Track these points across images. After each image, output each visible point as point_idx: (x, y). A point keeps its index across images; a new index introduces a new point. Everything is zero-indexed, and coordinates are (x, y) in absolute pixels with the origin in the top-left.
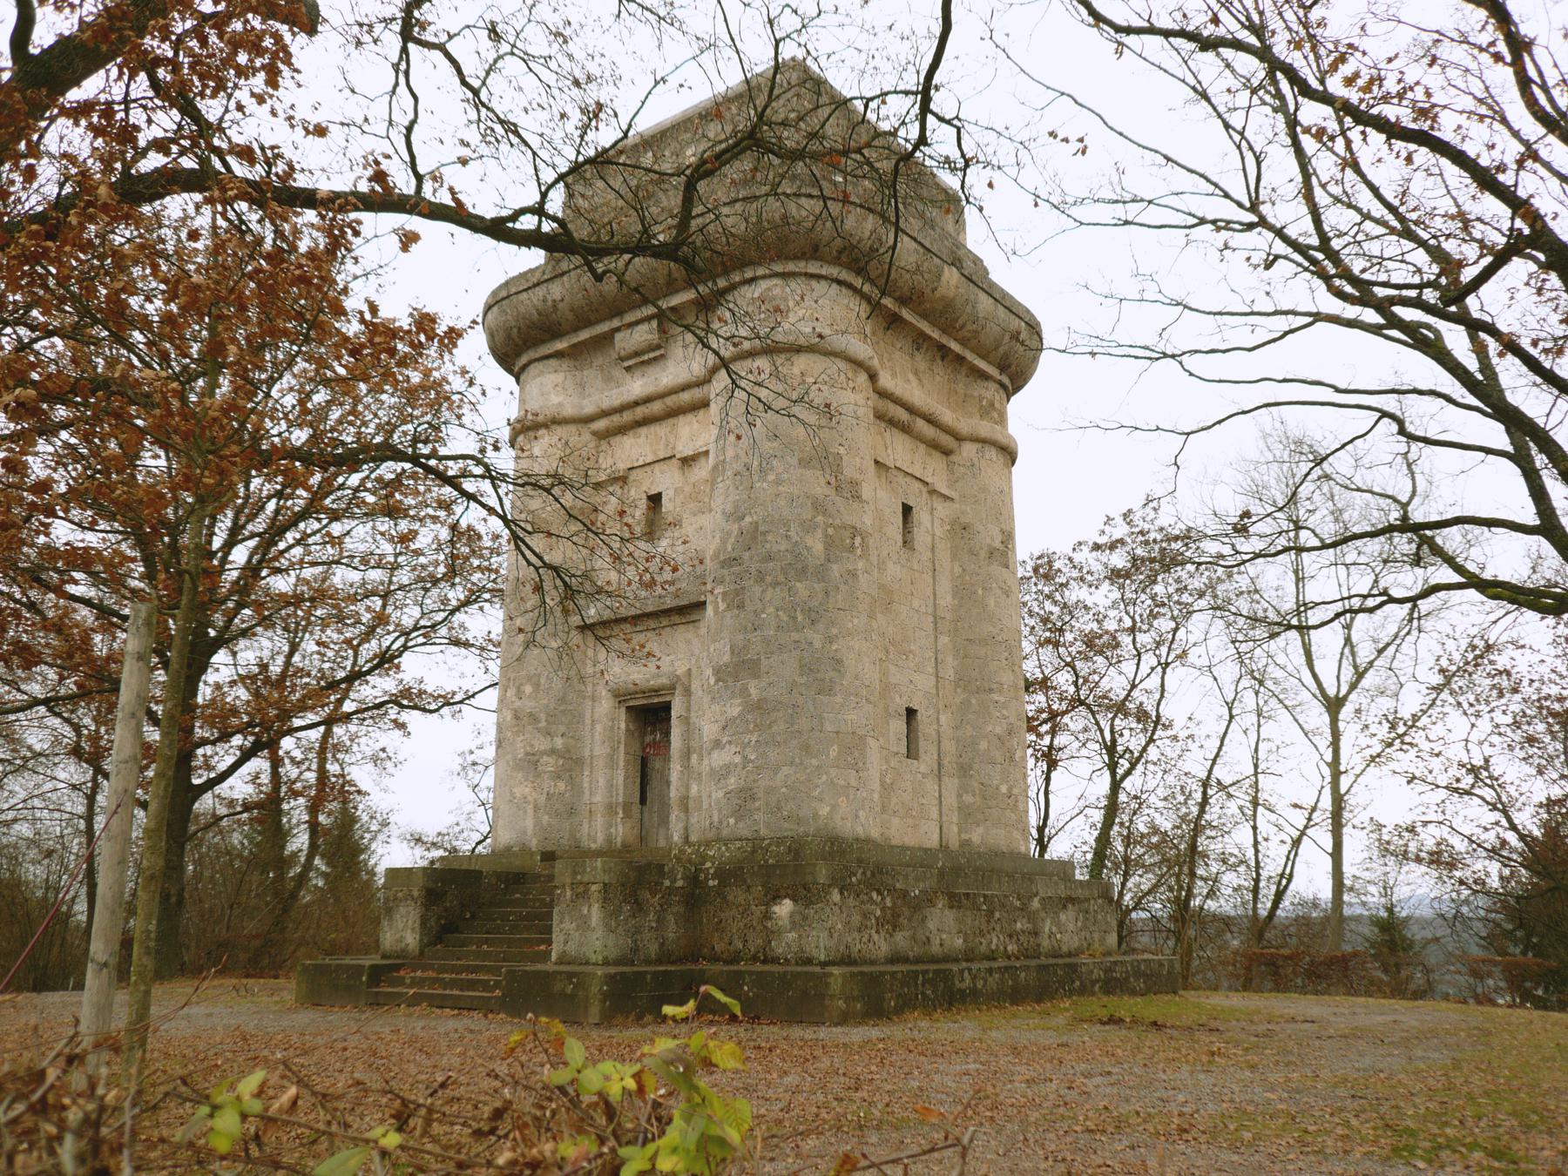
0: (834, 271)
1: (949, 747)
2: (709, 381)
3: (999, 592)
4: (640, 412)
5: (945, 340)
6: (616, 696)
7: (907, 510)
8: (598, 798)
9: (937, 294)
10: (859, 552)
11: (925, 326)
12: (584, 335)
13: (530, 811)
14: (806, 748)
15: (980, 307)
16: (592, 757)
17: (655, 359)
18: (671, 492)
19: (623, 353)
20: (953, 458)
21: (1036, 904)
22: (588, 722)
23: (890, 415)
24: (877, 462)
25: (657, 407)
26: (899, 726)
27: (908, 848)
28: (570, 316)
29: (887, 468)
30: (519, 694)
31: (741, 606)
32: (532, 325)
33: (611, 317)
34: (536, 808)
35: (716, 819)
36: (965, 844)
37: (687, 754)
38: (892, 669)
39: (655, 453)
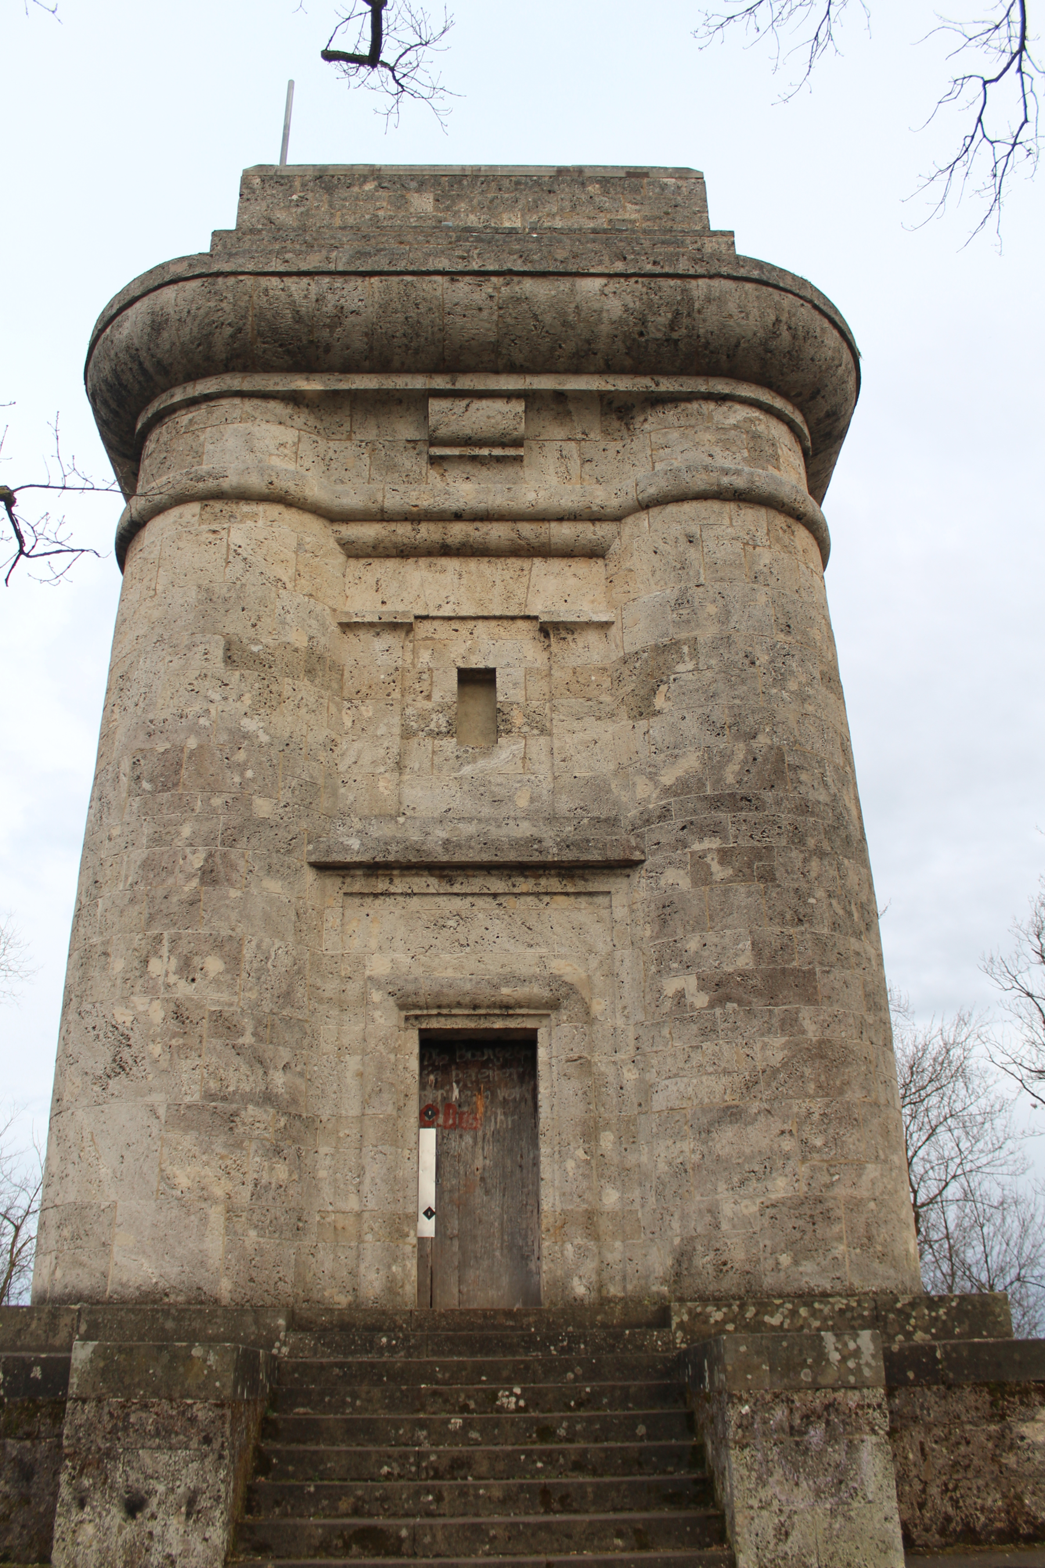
6: (402, 1007)
13: (216, 1215)
17: (499, 459)
18: (518, 674)
19: (443, 432)
22: (329, 1048)
25: (497, 533)
28: (359, 343)
34: (231, 1213)
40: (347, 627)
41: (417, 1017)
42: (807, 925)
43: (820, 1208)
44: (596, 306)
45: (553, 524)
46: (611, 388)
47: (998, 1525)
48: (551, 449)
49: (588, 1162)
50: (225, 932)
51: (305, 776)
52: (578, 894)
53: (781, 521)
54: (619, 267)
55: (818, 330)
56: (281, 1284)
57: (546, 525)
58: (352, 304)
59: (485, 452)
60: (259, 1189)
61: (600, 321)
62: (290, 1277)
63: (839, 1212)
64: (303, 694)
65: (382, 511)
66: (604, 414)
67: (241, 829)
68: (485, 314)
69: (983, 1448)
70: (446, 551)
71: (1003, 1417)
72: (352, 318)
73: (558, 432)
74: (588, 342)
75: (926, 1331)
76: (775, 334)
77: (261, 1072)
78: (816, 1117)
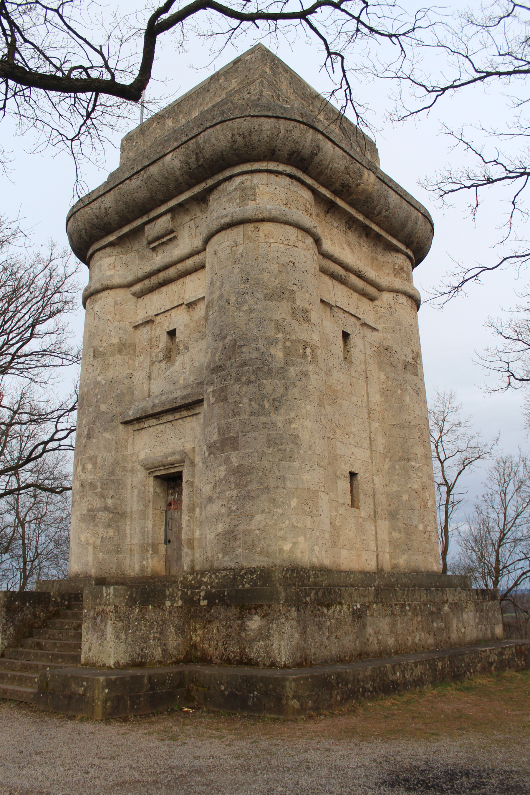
0: (289, 169)
1: (382, 499)
2: (204, 250)
3: (412, 392)
4: (162, 276)
5: (368, 222)
6: (147, 469)
7: (346, 336)
8: (135, 541)
10: (310, 358)
12: (126, 229)
13: (90, 548)
14: (273, 501)
15: (390, 200)
16: (132, 512)
17: (170, 240)
18: (182, 328)
20: (376, 303)
21: (446, 608)
22: (129, 487)
23: (332, 270)
24: (322, 301)
25: (172, 272)
26: (344, 485)
27: (352, 572)
28: (116, 217)
29: (331, 307)
30: (84, 469)
32: (94, 226)
33: (141, 215)
34: (95, 548)
35: (209, 554)
36: (395, 566)
37: (192, 509)
38: (339, 444)
39: (172, 302)
40: (136, 327)
41: (152, 472)
42: (237, 417)
43: (232, 535)
44: (171, 166)
45: (187, 261)
46: (192, 194)
47: (237, 658)
48: (187, 228)
49: (189, 520)
50: (93, 454)
51: (119, 392)
52: (192, 415)
54: (176, 144)
55: (257, 126)
56: (111, 570)
58: (107, 206)
59: (164, 240)
60: (103, 539)
61: (175, 171)
62: (115, 567)
63: (240, 536)
64: (117, 360)
65: (138, 278)
66: (198, 204)
67: (96, 417)
68: (142, 188)
69: (236, 630)
70: (161, 285)
71: (243, 618)
72: (110, 210)
73: (187, 218)
74: (176, 181)
75: (249, 584)
76: (235, 142)
77: (103, 500)
78: (234, 497)
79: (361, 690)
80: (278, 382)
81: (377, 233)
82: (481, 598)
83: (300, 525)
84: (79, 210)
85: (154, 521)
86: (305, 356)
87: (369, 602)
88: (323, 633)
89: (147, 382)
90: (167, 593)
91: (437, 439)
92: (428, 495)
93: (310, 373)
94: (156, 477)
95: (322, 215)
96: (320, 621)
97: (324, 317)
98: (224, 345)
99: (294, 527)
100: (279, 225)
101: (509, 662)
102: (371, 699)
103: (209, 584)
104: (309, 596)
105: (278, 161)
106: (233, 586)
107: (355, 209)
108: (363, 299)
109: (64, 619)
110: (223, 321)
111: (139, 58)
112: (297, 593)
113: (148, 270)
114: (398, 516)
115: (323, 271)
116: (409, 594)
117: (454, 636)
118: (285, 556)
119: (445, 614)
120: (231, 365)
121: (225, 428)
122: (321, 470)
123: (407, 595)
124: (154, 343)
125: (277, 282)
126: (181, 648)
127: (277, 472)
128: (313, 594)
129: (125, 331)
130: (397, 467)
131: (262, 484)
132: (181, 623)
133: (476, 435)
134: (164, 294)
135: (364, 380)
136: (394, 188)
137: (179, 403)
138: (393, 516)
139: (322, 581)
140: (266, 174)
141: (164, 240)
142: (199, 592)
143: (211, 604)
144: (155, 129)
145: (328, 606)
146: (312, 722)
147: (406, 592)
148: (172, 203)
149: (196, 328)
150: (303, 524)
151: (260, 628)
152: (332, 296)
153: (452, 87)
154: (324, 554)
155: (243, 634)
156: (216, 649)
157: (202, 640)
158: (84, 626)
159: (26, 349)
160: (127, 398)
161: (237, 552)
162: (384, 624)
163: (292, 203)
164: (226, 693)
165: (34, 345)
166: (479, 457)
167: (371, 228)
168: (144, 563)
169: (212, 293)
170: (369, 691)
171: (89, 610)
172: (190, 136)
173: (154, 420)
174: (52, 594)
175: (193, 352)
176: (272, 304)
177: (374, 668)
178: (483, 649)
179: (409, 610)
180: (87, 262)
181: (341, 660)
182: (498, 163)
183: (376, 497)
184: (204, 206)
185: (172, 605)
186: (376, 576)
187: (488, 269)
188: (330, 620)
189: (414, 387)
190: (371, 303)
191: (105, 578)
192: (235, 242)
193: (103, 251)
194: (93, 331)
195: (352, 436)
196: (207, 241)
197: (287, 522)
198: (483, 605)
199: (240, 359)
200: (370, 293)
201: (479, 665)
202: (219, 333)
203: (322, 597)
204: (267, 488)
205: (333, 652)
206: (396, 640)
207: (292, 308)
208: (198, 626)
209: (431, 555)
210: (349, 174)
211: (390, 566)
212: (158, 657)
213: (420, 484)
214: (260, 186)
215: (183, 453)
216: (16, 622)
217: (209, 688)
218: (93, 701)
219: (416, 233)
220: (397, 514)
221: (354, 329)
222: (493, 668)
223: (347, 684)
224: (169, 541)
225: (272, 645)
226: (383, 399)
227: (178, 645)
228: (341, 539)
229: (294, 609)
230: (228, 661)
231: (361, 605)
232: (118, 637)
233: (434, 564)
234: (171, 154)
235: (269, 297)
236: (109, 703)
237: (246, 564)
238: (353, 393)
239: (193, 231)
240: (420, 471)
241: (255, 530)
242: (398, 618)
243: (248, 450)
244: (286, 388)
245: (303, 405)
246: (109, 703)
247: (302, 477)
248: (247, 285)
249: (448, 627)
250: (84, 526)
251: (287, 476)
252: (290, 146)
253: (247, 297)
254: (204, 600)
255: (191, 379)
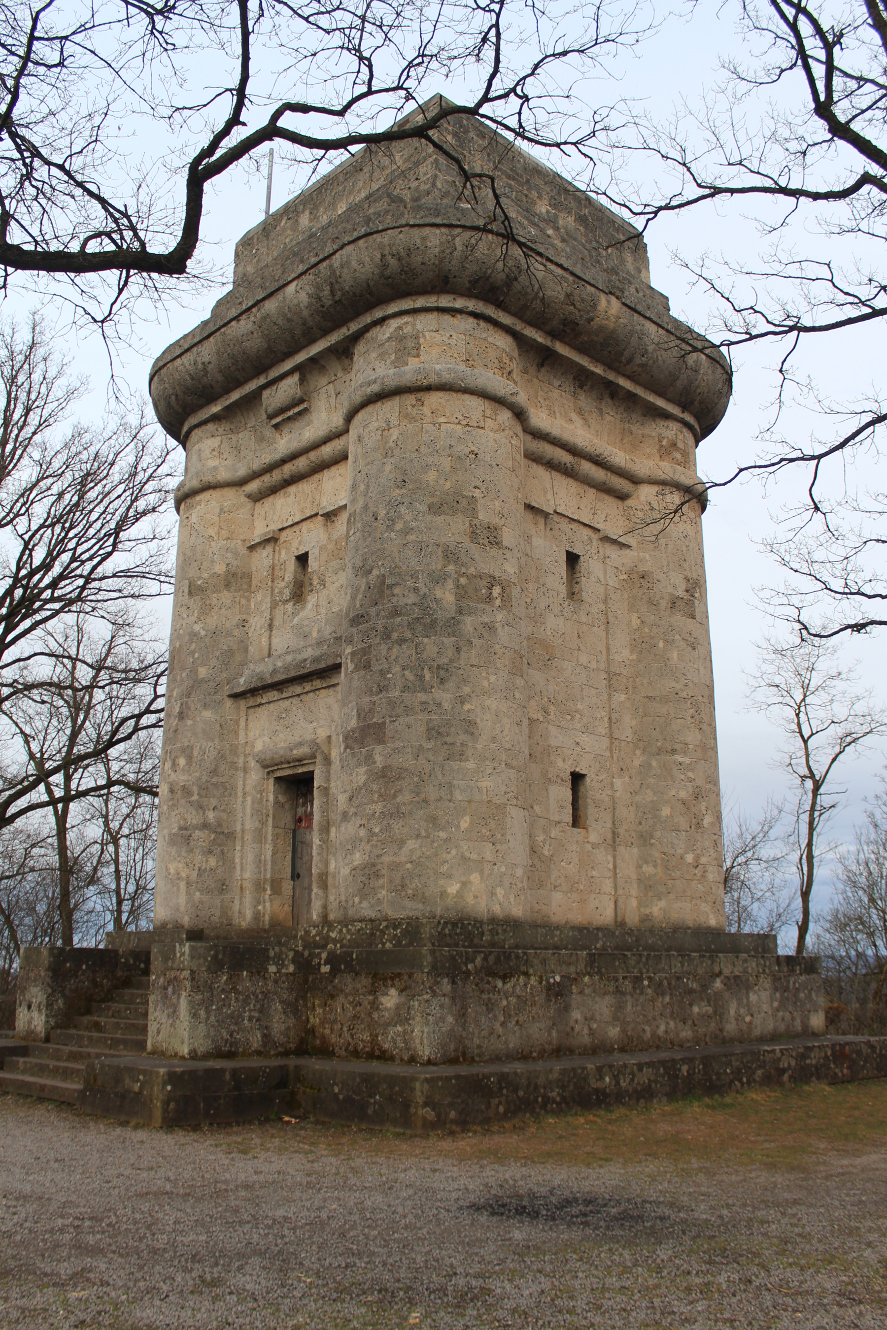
0: (471, 305)
1: (627, 814)
2: (347, 431)
3: (683, 644)
4: (288, 469)
5: (611, 376)
6: (265, 767)
7: (572, 559)
8: (247, 875)
9: (595, 324)
10: (498, 602)
11: (584, 361)
12: (235, 396)
13: (183, 885)
14: (433, 820)
17: (300, 413)
20: (629, 502)
22: (240, 794)
23: (548, 457)
24: (529, 507)
25: (302, 463)
28: (219, 377)
29: (546, 515)
30: (174, 764)
31: (367, 666)
34: (189, 884)
35: (343, 898)
36: (646, 919)
37: (325, 829)
38: (553, 730)
40: (252, 548)
43: (374, 869)
44: (295, 302)
45: (323, 447)
48: (323, 396)
52: (328, 687)
53: (410, 399)
54: (301, 268)
55: (418, 241)
57: (319, 450)
58: (206, 359)
59: (291, 413)
61: (301, 310)
63: (384, 872)
65: (254, 472)
66: (339, 359)
67: (192, 687)
73: (323, 381)
74: (304, 324)
76: (385, 266)
79: (540, 1099)
80: (445, 640)
81: (629, 392)
82: (785, 969)
83: (474, 856)
84: (165, 365)
85: (275, 845)
86: (489, 598)
87: (577, 973)
88: (495, 1016)
89: (267, 634)
90: (272, 954)
91: (798, 702)
92: (703, 808)
93: (497, 625)
94: (278, 780)
95: (532, 370)
96: (489, 999)
97: (533, 532)
98: (368, 583)
99: (464, 858)
100: (454, 395)
101: (817, 1069)
102: (556, 1113)
103: (338, 941)
104: (473, 961)
105: (454, 293)
106: (371, 945)
107: (588, 356)
108: (606, 497)
109: (138, 988)
110: (367, 546)
111: (181, 214)
112: (453, 958)
113: (267, 461)
114: (653, 841)
115: (533, 458)
116: (650, 963)
117: (731, 1027)
118: (449, 902)
119: (715, 994)
120: (378, 615)
121: (367, 709)
122: (512, 773)
123: (646, 963)
124: (278, 573)
125: (448, 485)
126: (292, 1033)
127: (440, 776)
128: (479, 960)
129: (236, 554)
130: (654, 763)
131: (418, 794)
132: (292, 998)
133: (866, 694)
134: (292, 497)
135: (603, 627)
136: (655, 319)
137: (309, 667)
138: (645, 840)
139: (504, 940)
140: (435, 314)
141: (291, 413)
142: (320, 954)
143: (334, 972)
144: (284, 230)
145: (505, 978)
146: (450, 1140)
147: (644, 959)
148: (301, 357)
149: (336, 552)
150: (479, 854)
151: (398, 1007)
152: (550, 496)
153: (667, 207)
154: (512, 900)
155: (375, 1015)
156: (340, 1036)
157: (322, 1023)
158: (152, 998)
159: (108, 567)
160: (238, 658)
161: (379, 896)
162: (603, 1007)
163: (476, 358)
164: (341, 1097)
165: (118, 561)
166: (871, 732)
167: (618, 385)
168: (260, 907)
169: (353, 501)
170: (554, 1101)
171: (158, 977)
172: (321, 257)
173: (275, 693)
174: (121, 952)
175: (332, 588)
176: (439, 520)
177: (564, 1070)
178: (768, 1049)
179: (649, 986)
180: (183, 441)
181: (524, 1056)
182: (756, 312)
183: (617, 811)
184: (347, 362)
185: (279, 971)
186: (600, 934)
187: (717, 485)
188: (507, 998)
189: (687, 637)
190: (620, 502)
191: (202, 930)
192: (388, 422)
193: (204, 427)
194: (189, 553)
195: (578, 716)
196: (349, 418)
197: (454, 852)
198: (788, 982)
199: (390, 605)
200: (618, 487)
201: (759, 1072)
202: (361, 564)
203: (495, 963)
204: (425, 801)
205: (511, 1045)
206: (624, 1031)
207: (471, 526)
208: (317, 1002)
209: (706, 901)
210: (573, 305)
211: (637, 919)
212: (255, 1045)
213: (691, 790)
214: (427, 334)
215: (314, 743)
216: (67, 992)
217: (319, 1090)
218: (151, 1101)
219: (697, 387)
220: (652, 837)
221: (587, 548)
222: (786, 1077)
223: (516, 1091)
224: (298, 876)
225: (413, 1031)
226: (634, 657)
227: (288, 1028)
228: (553, 877)
229: (446, 980)
230: (356, 1054)
231: (562, 977)
232: (195, 1014)
233: (711, 916)
234: (295, 283)
235: (435, 509)
236: (172, 1105)
237: (391, 913)
238: (583, 648)
239: (332, 400)
240: (692, 770)
241: (406, 863)
242: (628, 997)
243: (399, 744)
244: (458, 650)
245: (484, 674)
246: (172, 1105)
247: (480, 784)
248: (404, 491)
249: (719, 1013)
250: (174, 851)
251: (455, 782)
252: (472, 268)
253: (402, 509)
254: (325, 964)
255: (328, 631)
